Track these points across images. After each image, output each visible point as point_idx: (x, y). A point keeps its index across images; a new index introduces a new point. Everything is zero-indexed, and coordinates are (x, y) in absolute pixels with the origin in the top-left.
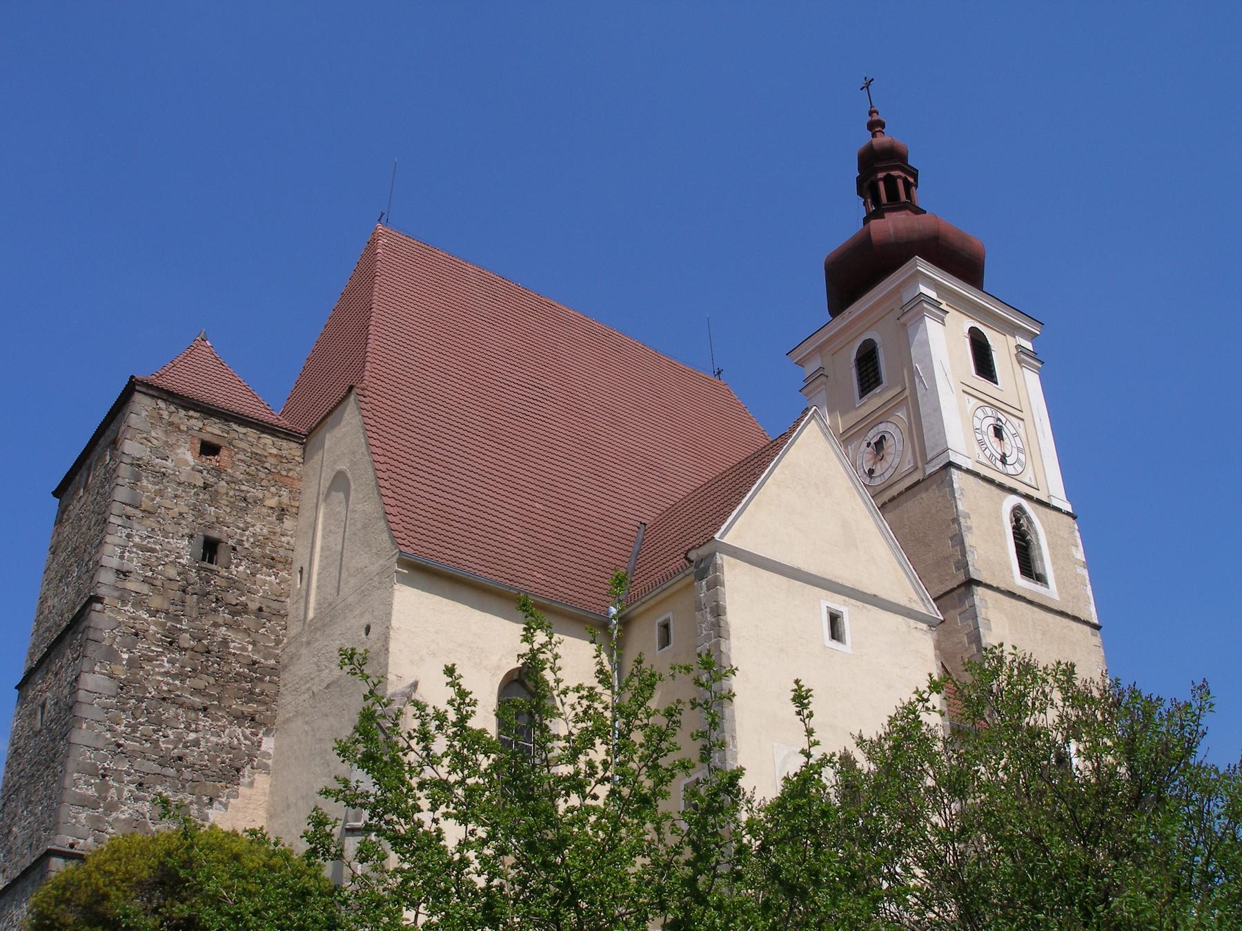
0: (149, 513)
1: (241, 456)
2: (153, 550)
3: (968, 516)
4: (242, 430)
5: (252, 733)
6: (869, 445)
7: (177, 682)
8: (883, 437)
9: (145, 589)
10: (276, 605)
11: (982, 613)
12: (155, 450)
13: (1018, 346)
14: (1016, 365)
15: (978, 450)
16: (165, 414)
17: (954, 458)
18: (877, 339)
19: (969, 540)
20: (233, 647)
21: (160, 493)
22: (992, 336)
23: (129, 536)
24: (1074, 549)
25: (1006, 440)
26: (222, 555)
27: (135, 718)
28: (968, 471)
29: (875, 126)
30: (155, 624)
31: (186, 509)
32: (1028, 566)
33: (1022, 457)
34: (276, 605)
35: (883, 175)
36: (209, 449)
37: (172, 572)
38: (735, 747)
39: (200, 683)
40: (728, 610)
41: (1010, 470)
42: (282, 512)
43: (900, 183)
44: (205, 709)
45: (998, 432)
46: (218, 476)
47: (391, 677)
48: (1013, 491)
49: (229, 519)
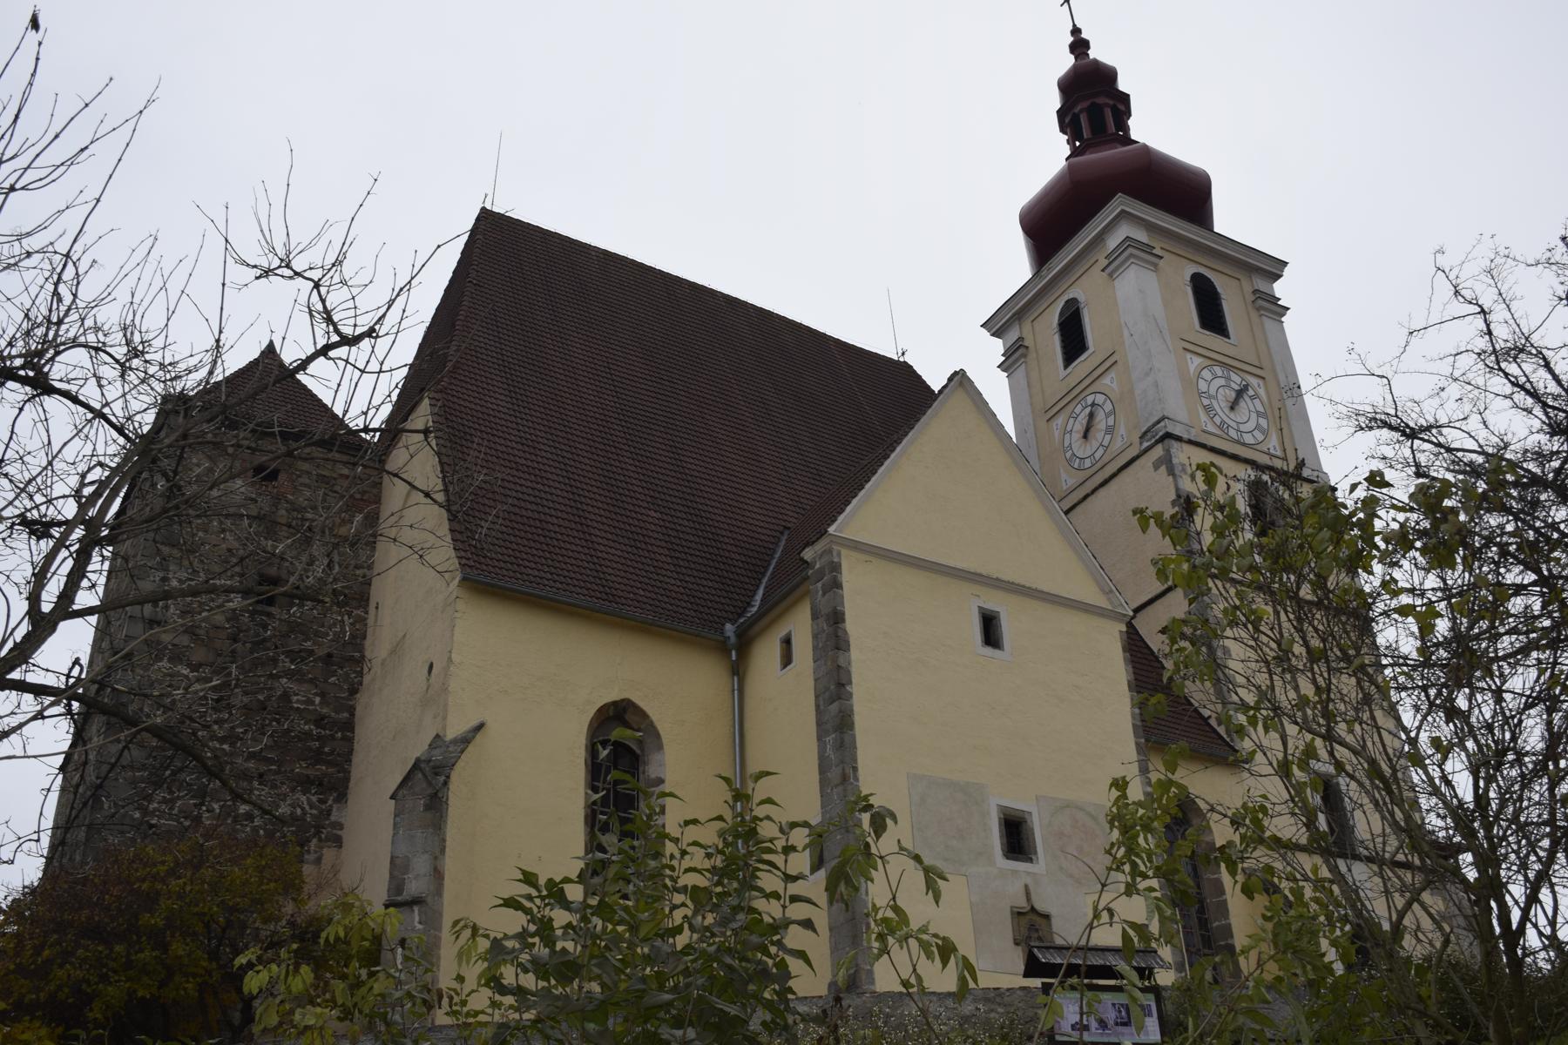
5: (320, 801)
7: (225, 747)
9: (185, 640)
13: (1255, 291)
14: (1254, 315)
15: (1203, 417)
18: (1081, 298)
20: (297, 701)
22: (1219, 282)
27: (171, 792)
28: (1190, 442)
29: (1079, 46)
35: (1091, 99)
38: (857, 779)
40: (847, 617)
43: (1108, 113)
44: (261, 776)
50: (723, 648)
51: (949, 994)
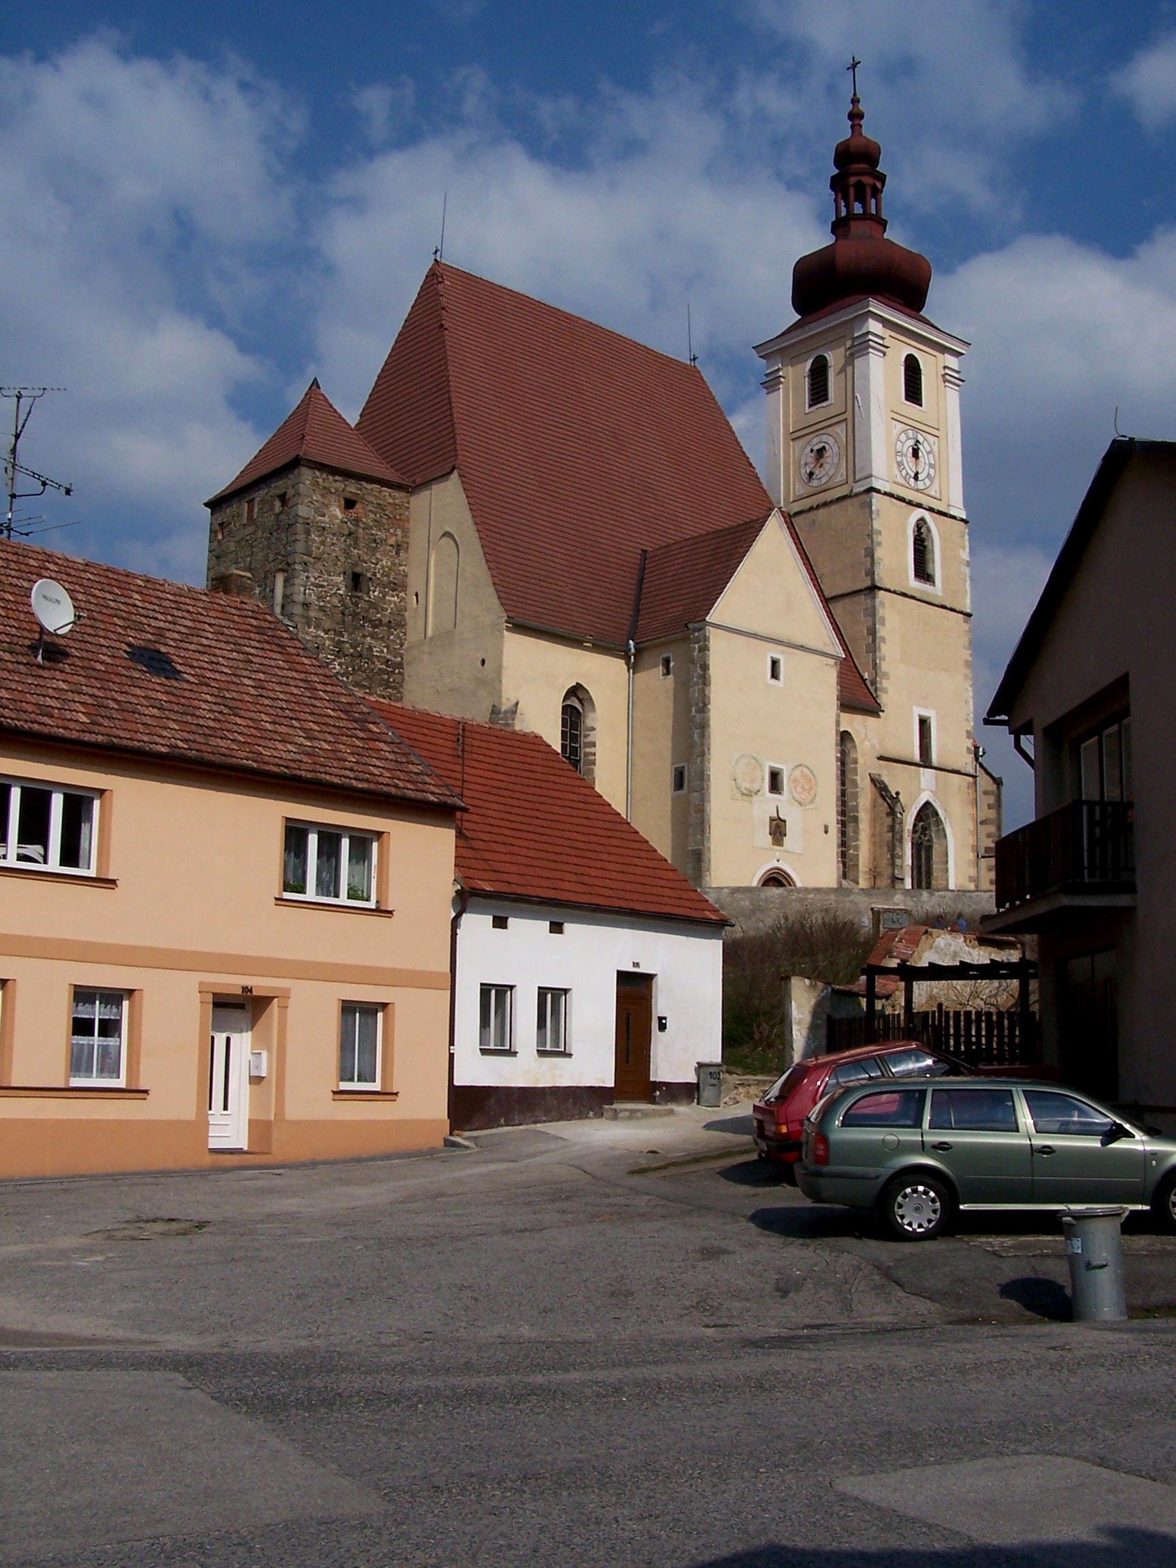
0: (318, 559)
1: (370, 508)
2: (323, 586)
3: (879, 533)
4: (369, 486)
6: (812, 451)
8: (824, 448)
9: (320, 615)
10: (398, 618)
11: (880, 612)
12: (316, 510)
16: (320, 480)
17: (876, 485)
19: (879, 553)
21: (323, 543)
23: (308, 577)
24: (961, 551)
25: (921, 459)
26: (363, 585)
28: (885, 494)
30: (329, 639)
31: (339, 553)
32: (923, 572)
33: (932, 472)
34: (398, 618)
36: (349, 504)
37: (335, 601)
39: (358, 678)
41: (920, 485)
42: (398, 547)
45: (915, 453)
46: (357, 525)
47: (504, 700)
48: (919, 506)
49: (366, 558)
50: (626, 658)
51: (832, 889)
